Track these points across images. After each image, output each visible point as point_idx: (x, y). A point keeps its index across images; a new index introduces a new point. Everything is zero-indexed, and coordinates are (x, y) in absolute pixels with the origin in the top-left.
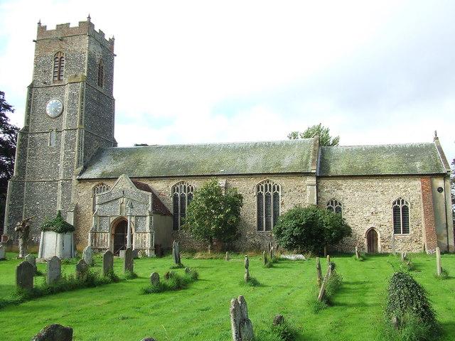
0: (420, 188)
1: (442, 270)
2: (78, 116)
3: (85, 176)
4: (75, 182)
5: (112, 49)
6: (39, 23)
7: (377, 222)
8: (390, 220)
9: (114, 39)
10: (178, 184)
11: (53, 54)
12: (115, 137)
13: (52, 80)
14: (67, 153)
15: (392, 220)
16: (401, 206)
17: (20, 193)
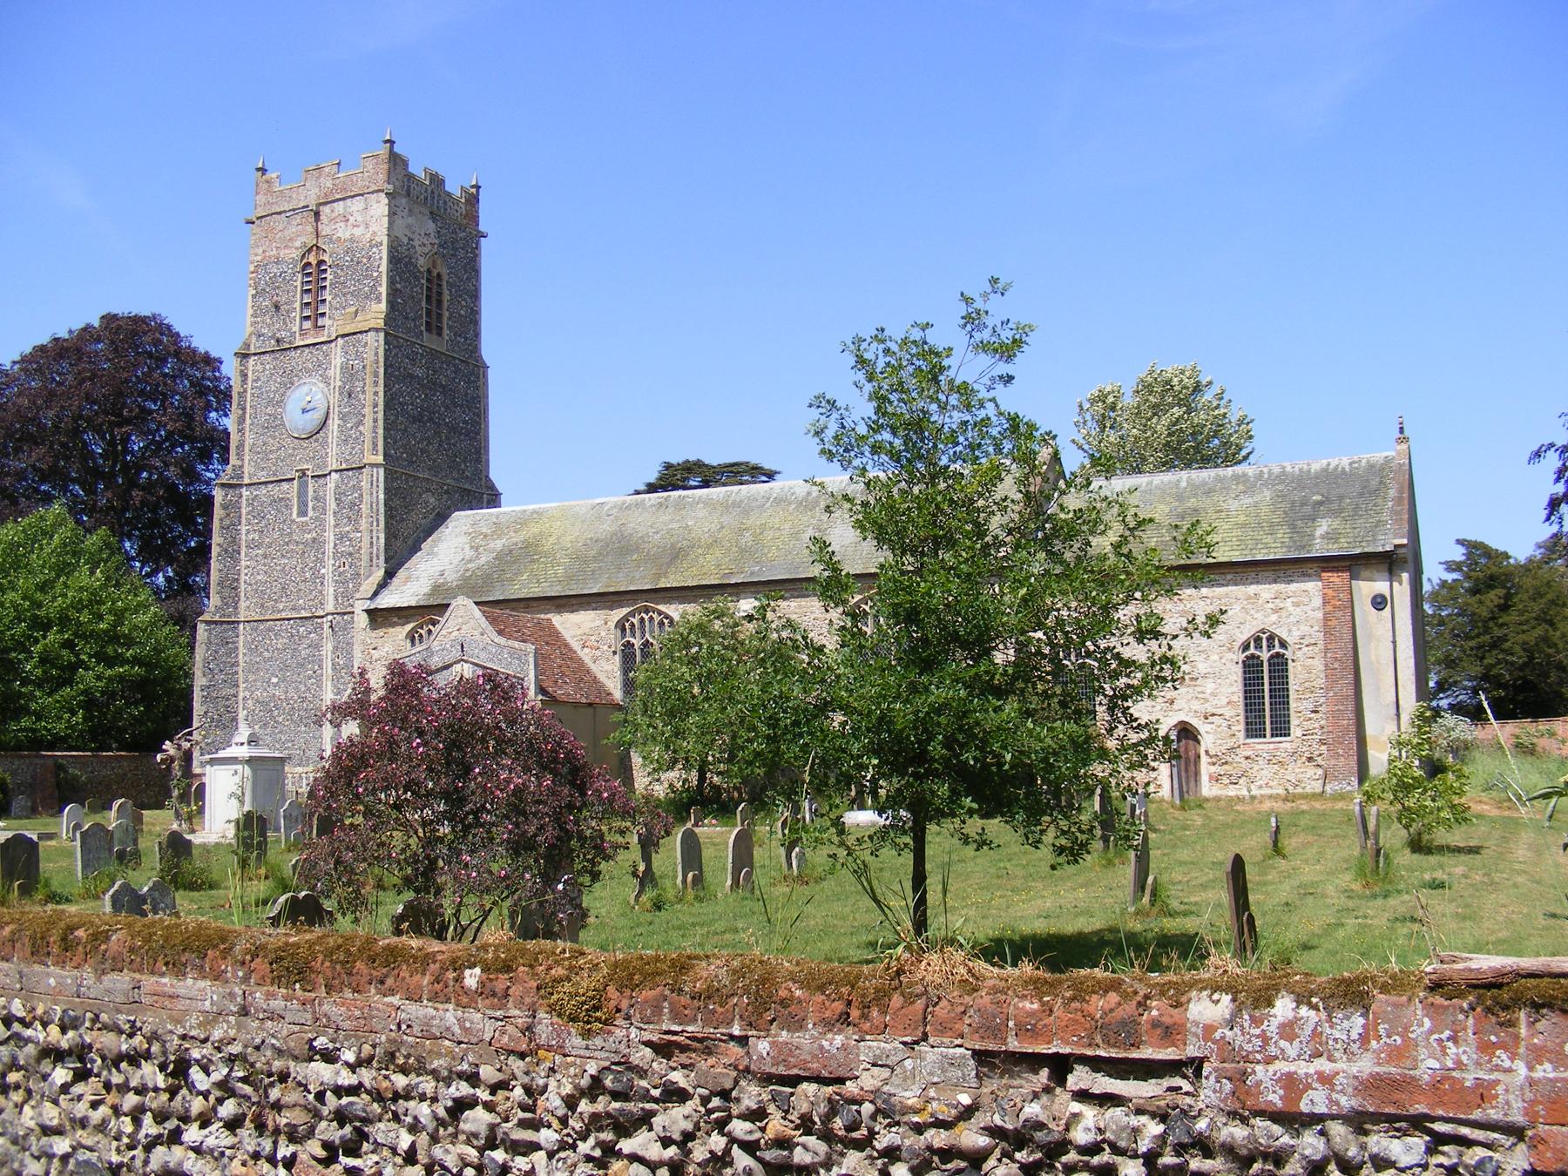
0: (1317, 601)
2: (366, 428)
3: (387, 600)
4: (362, 620)
5: (474, 218)
6: (396, 161)
7: (1196, 706)
8: (1235, 698)
10: (632, 614)
11: (296, 254)
12: (493, 476)
13: (296, 329)
14: (341, 537)
15: (1239, 698)
16: (1265, 655)
17: (228, 654)
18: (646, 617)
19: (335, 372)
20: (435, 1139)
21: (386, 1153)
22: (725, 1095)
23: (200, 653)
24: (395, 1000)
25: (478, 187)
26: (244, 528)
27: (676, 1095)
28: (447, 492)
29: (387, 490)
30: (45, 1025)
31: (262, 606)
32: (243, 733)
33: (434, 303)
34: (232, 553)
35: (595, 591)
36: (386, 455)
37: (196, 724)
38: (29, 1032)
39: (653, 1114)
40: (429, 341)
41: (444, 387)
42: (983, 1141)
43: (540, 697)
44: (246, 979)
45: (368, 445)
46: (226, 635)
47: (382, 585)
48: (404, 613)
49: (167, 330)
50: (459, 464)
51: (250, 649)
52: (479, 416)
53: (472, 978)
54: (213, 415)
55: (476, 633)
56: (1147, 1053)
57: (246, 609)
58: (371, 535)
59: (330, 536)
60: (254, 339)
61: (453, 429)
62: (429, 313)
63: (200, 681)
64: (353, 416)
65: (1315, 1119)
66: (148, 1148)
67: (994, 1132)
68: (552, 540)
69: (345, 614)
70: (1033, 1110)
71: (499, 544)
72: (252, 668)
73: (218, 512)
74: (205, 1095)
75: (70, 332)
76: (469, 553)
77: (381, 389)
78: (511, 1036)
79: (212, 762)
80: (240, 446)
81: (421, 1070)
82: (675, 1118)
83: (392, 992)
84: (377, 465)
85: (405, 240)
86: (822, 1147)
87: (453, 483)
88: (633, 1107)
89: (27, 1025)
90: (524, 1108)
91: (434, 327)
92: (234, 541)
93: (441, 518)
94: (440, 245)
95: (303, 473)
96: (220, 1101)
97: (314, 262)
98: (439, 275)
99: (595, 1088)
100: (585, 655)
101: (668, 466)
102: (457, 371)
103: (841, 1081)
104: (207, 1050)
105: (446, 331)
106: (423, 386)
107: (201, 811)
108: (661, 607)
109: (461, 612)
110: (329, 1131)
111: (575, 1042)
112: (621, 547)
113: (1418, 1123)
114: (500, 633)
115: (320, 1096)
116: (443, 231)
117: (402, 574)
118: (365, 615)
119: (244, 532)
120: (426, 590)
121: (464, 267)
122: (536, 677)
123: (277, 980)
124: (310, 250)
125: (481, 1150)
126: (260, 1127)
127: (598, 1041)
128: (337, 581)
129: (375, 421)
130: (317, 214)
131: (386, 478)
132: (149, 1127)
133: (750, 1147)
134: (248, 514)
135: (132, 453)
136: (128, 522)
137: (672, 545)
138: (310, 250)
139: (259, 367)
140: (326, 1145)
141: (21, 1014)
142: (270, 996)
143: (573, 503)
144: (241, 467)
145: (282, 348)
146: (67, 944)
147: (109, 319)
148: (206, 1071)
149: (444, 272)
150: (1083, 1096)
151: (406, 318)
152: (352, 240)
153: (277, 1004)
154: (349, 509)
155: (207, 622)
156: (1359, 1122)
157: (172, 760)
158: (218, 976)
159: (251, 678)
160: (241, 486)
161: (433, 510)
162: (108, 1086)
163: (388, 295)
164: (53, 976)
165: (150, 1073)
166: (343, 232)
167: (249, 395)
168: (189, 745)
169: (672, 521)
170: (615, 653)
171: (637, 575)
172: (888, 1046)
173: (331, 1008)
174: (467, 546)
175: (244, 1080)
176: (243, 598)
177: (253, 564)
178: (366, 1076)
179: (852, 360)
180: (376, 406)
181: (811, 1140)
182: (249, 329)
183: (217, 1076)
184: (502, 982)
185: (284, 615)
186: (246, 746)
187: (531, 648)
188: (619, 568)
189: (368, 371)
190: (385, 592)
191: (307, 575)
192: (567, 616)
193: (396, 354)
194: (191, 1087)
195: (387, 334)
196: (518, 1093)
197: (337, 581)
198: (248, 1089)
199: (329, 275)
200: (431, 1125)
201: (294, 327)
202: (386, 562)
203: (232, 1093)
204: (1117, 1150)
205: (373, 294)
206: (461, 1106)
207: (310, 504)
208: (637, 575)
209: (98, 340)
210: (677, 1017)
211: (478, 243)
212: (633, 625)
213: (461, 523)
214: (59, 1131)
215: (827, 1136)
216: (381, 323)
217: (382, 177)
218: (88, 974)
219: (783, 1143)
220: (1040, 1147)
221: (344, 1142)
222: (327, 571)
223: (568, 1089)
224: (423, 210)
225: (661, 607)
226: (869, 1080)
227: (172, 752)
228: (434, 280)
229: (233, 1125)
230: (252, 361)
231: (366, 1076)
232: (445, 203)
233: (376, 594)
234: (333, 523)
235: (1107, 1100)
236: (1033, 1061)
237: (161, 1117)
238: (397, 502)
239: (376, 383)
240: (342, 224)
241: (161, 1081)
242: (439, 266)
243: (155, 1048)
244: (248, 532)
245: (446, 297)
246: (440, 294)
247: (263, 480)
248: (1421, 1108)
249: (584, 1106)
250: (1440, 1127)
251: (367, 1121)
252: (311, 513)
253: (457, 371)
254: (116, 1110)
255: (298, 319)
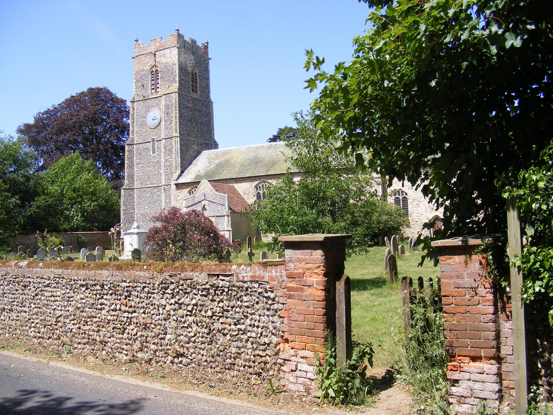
1: (508, 406)
2: (173, 124)
3: (182, 180)
4: (174, 187)
5: (206, 53)
6: (180, 36)
9: (323, 61)
10: (259, 183)
11: (149, 68)
13: (149, 92)
14: (166, 160)
17: (132, 199)
18: (264, 184)
19: (162, 106)
20: (141, 293)
21: (134, 296)
22: (178, 282)
23: (122, 199)
24: (134, 271)
25: (207, 43)
26: (135, 158)
27: (172, 283)
28: (200, 144)
29: (181, 145)
30: (80, 281)
31: (142, 183)
32: (135, 225)
33: (194, 82)
34: (132, 166)
35: (247, 176)
36: (180, 133)
37: (121, 222)
38: (78, 282)
39: (169, 286)
40: (193, 95)
41: (198, 110)
42: (209, 287)
43: (230, 211)
44: (112, 270)
45: (174, 130)
46: (130, 193)
47: (180, 176)
48: (187, 184)
49: (108, 92)
50: (204, 135)
51: (138, 197)
52: (210, 119)
53: (145, 267)
54: (125, 119)
55: (209, 191)
56: (227, 273)
57: (136, 185)
58: (176, 159)
59: (163, 160)
60: (136, 96)
61: (202, 123)
62: (193, 86)
63: (122, 208)
64: (169, 121)
65: (246, 282)
66: (98, 300)
67: (210, 285)
68: (234, 159)
69: (168, 185)
70: (215, 282)
71: (217, 161)
72: (139, 203)
73: (127, 153)
74: (107, 290)
75: (77, 94)
76: (208, 164)
77: (178, 112)
78: (151, 276)
79: (126, 234)
80: (133, 132)
81: (138, 283)
82: (172, 287)
83: (134, 270)
84: (177, 137)
85: (184, 62)
86: (190, 289)
87: (203, 141)
88: (167, 285)
89: (78, 281)
90: (153, 287)
91: (194, 90)
92: (132, 162)
93: (199, 153)
94: (196, 63)
95: (154, 140)
96: (109, 291)
97: (155, 71)
98: (196, 73)
99: (162, 283)
100: (245, 197)
101: (280, 130)
102: (203, 104)
103: (192, 279)
104: (107, 282)
105: (198, 92)
106: (191, 110)
107: (123, 250)
108: (269, 181)
109: (204, 184)
110: (126, 294)
111: (159, 276)
112: (256, 161)
113: (257, 282)
114: (217, 191)
115: (124, 288)
116: (197, 58)
117: (186, 172)
118: (175, 185)
119: (135, 159)
120: (194, 177)
121: (204, 70)
122: (228, 204)
123: (117, 270)
124: (153, 67)
125: (147, 294)
126: (115, 294)
127: (162, 276)
128: (165, 175)
129: (176, 122)
130: (155, 55)
131: (180, 141)
132: (98, 296)
133: (182, 290)
134: (136, 153)
135: (98, 132)
136: (98, 156)
137: (273, 160)
138: (153, 67)
139: (138, 106)
140: (125, 296)
141: (76, 279)
142: (116, 272)
143: (241, 147)
144: (134, 138)
145: (145, 99)
146: (84, 266)
147: (91, 90)
148: (107, 286)
149: (197, 72)
150: (221, 280)
151: (185, 88)
152: (167, 63)
153: (117, 274)
154: (169, 151)
155: (124, 189)
156: (251, 282)
157: (113, 234)
158: (108, 270)
159: (139, 206)
160: (133, 144)
161: (196, 150)
162: (91, 290)
163: (179, 80)
164: (82, 272)
165: (98, 287)
166: (164, 60)
167: (135, 115)
168: (118, 229)
169: (272, 152)
170: (254, 196)
171: (261, 171)
172: (197, 274)
173: (125, 273)
174: (207, 163)
175: (113, 287)
176: (135, 181)
177: (138, 170)
178: (131, 284)
179: (293, 118)
180: (176, 117)
181: (189, 288)
182: (134, 93)
183: (108, 287)
184: (149, 268)
185: (149, 186)
186: (136, 229)
187: (226, 195)
188: (255, 168)
189: (173, 106)
190: (181, 178)
191: (156, 173)
192: (239, 184)
193: (182, 100)
194: (104, 289)
195: (179, 93)
196: (152, 284)
197: (165, 175)
198: (113, 288)
199: (159, 75)
200: (140, 291)
201: (149, 92)
202: (181, 168)
203: (111, 289)
204: (225, 287)
205: (174, 81)
206: (144, 287)
207: (156, 150)
208: (261, 171)
209: (86, 96)
210: (172, 271)
211: (208, 62)
212: (260, 187)
213: (205, 154)
214: (83, 299)
215: (191, 288)
216: (177, 90)
217: (176, 42)
218: (87, 271)
219: (186, 289)
220: (216, 287)
221: (128, 295)
222: (162, 171)
223: (158, 283)
224: (189, 52)
225: (269, 181)
226: (195, 279)
227: (113, 231)
228: (194, 75)
229: (111, 294)
230: (136, 103)
231: (131, 284)
232: (197, 49)
233: (178, 178)
234: (163, 156)
235: (223, 280)
236: (215, 275)
237: (100, 295)
238: (184, 148)
239: (176, 110)
240: (163, 58)
241: (100, 288)
242: (195, 70)
243: (99, 283)
244: (136, 159)
245: (198, 80)
246: (196, 79)
247: (141, 142)
248: (257, 280)
249: (161, 286)
250: (259, 282)
251: (131, 291)
252: (156, 153)
253: (203, 104)
254: (93, 294)
255: (150, 89)
